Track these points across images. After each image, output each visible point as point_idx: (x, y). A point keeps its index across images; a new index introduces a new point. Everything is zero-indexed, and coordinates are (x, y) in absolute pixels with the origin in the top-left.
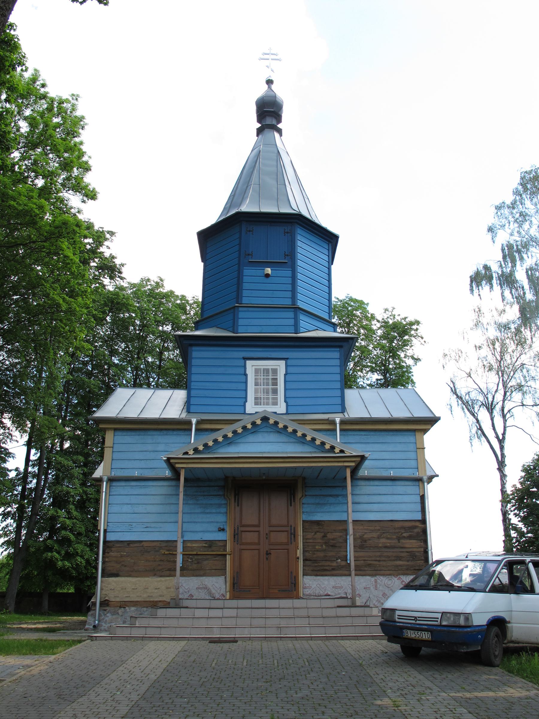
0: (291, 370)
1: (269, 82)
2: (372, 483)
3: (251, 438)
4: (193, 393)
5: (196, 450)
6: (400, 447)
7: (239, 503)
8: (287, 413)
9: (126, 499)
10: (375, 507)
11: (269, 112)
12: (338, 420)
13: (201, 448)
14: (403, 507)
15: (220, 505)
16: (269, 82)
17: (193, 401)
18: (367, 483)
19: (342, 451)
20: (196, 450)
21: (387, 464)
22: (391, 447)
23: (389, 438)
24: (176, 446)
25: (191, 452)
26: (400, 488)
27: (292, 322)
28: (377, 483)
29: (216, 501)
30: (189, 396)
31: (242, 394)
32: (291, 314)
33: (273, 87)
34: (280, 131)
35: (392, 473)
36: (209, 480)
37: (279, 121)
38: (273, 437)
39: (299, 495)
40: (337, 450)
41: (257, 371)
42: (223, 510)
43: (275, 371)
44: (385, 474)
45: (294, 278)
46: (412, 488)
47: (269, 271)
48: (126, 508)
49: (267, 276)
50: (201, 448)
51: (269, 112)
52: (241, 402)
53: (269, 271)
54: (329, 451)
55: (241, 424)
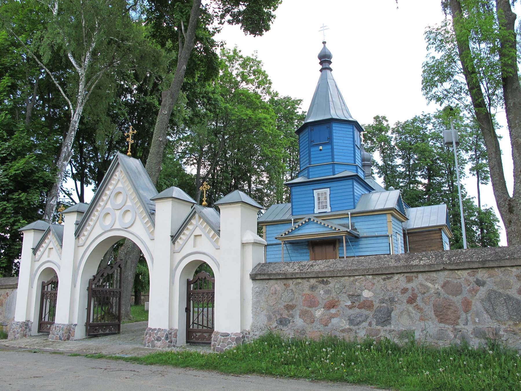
0: (332, 192)
1: (324, 43)
2: (367, 239)
3: (307, 227)
4: (294, 204)
5: (285, 234)
6: (380, 222)
7: (314, 251)
8: (331, 212)
9: (272, 253)
10: (369, 249)
11: (325, 59)
12: (349, 213)
13: (287, 233)
14: (381, 248)
15: (307, 253)
16: (324, 43)
17: (294, 207)
18: (365, 239)
19: (339, 230)
20: (285, 234)
21: (374, 230)
22: (376, 222)
23: (375, 218)
24: (283, 230)
25: (284, 235)
26: (380, 240)
27: (331, 170)
28: (370, 239)
29: (305, 251)
30: (292, 205)
31: (312, 205)
32: (331, 167)
33: (326, 45)
34: (331, 70)
35: (376, 234)
36: (302, 243)
37: (330, 63)
38: (314, 226)
39: (337, 246)
40: (337, 229)
41: (318, 194)
42: (308, 254)
43: (326, 193)
44: (373, 234)
45: (332, 149)
46: (385, 240)
47: (321, 147)
48: (272, 256)
49: (321, 150)
50: (287, 233)
51: (325, 59)
52: (312, 208)
53: (321, 147)
54: (334, 230)
55: (304, 220)
